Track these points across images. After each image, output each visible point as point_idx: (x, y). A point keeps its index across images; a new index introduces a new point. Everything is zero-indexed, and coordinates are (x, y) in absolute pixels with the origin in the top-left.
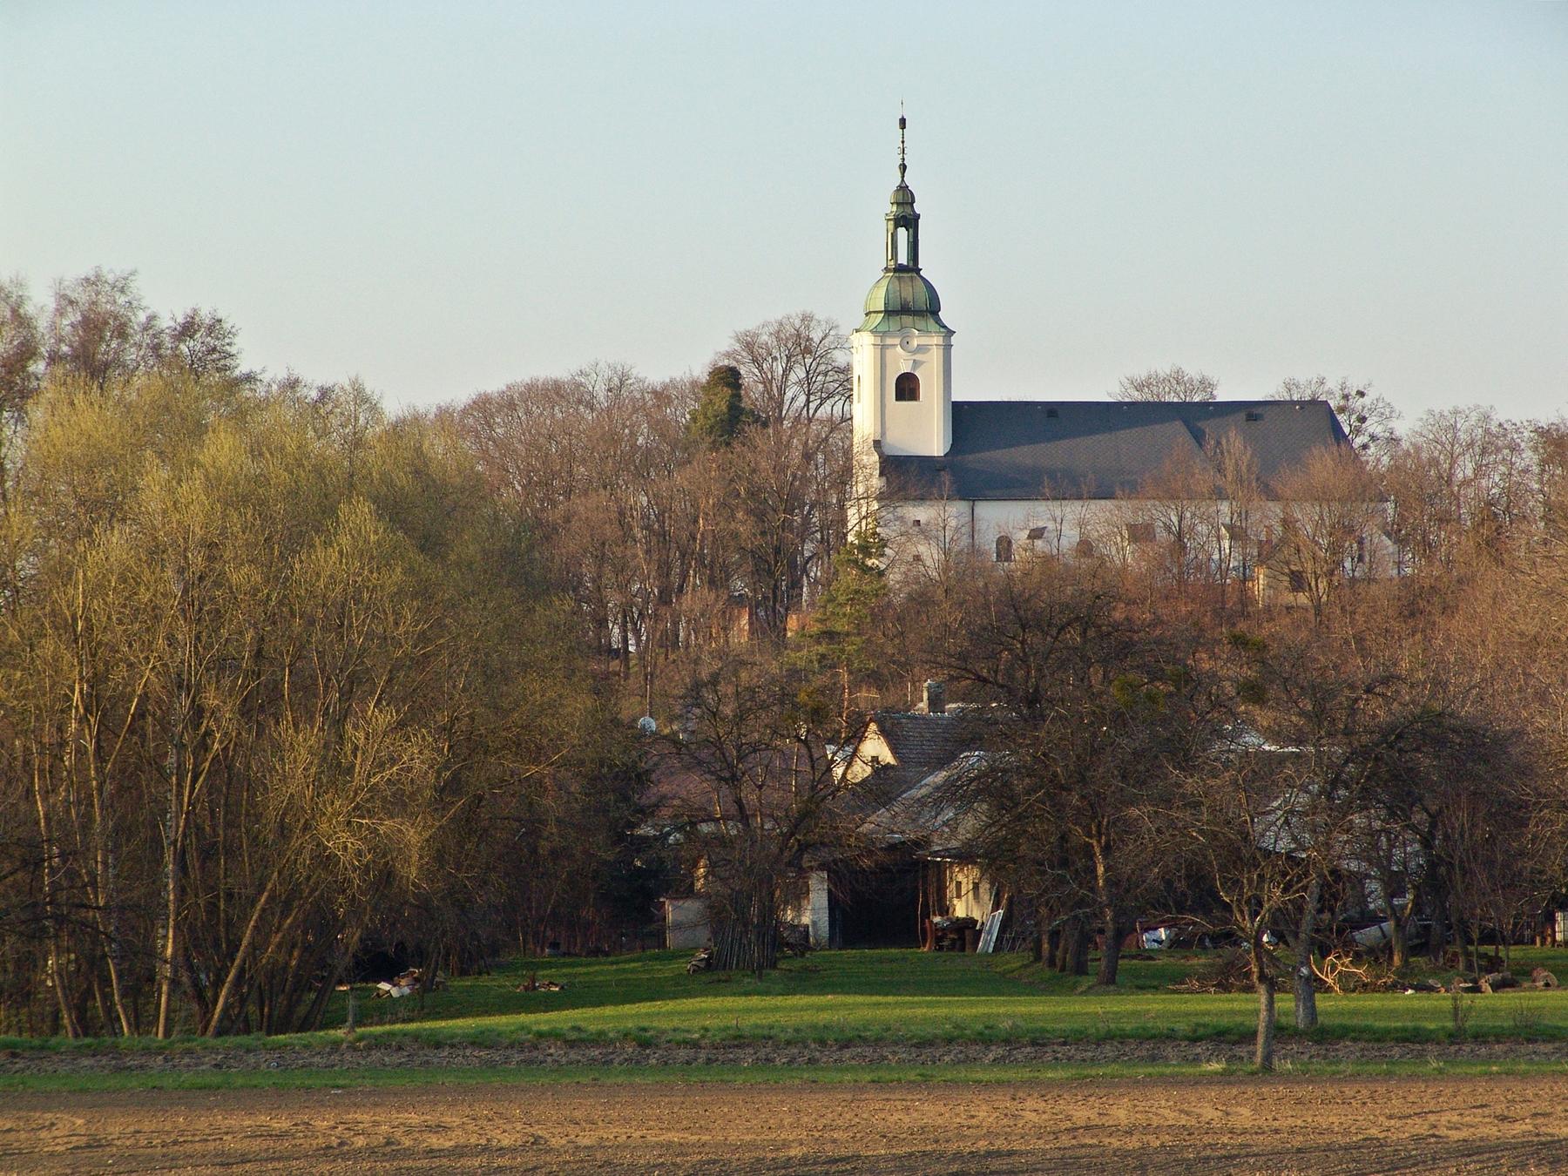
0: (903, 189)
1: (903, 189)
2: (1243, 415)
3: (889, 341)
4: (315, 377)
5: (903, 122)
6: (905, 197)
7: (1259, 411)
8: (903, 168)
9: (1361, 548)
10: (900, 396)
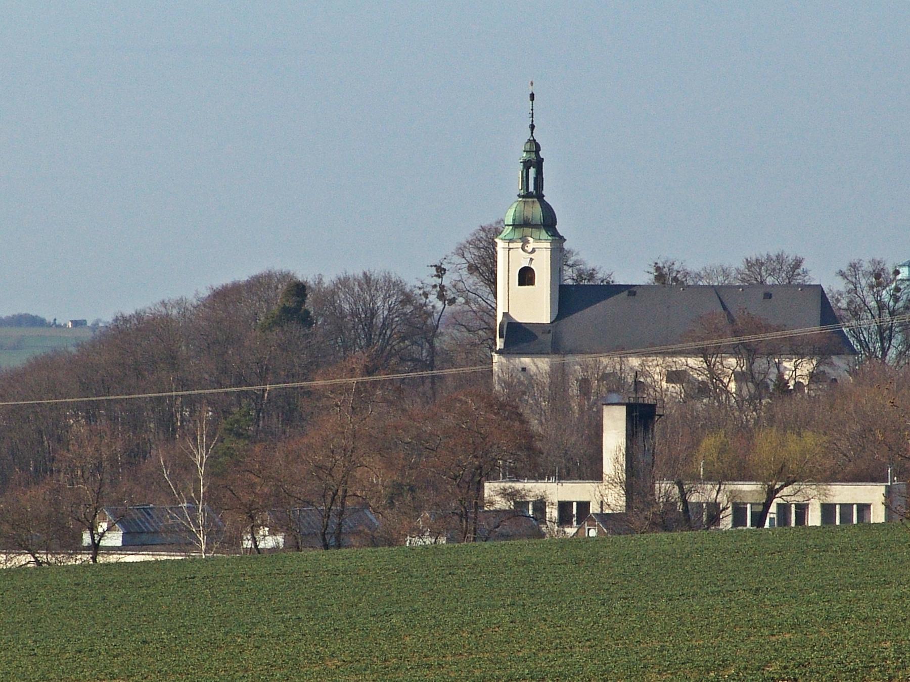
0: (533, 142)
1: (533, 142)
2: (626, 293)
3: (511, 245)
4: (356, 271)
5: (532, 96)
6: (534, 147)
7: (634, 289)
8: (532, 127)
9: (324, 539)
10: (521, 283)
